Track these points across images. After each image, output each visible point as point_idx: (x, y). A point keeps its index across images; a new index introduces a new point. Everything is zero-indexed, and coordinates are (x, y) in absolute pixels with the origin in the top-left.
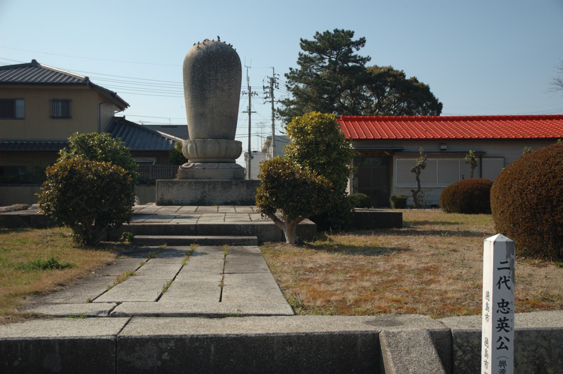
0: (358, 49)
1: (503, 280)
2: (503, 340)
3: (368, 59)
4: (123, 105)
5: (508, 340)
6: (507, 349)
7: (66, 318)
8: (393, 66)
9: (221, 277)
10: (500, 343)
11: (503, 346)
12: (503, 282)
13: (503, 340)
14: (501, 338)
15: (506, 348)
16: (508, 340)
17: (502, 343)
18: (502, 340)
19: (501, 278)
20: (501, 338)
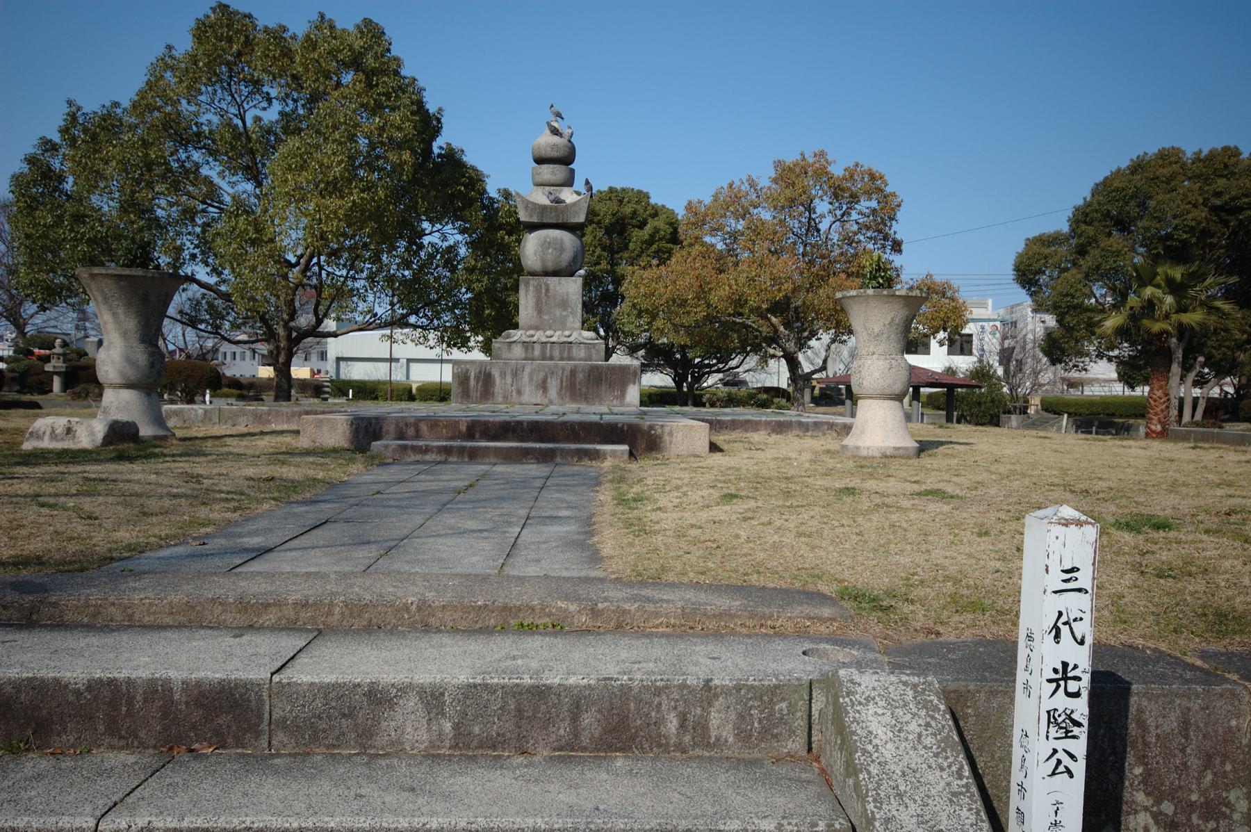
0: (941, 344)
1: (1064, 619)
2: (1061, 755)
3: (1201, 151)
4: (897, 247)
5: (1072, 756)
6: (1071, 776)
7: (169, 634)
8: (614, 185)
9: (508, 570)
10: (1053, 761)
11: (1061, 769)
12: (1064, 624)
13: (1061, 755)
14: (1055, 751)
15: (1069, 772)
16: (1072, 756)
17: (1059, 762)
18: (1057, 756)
19: (1060, 614)
20: (1055, 751)
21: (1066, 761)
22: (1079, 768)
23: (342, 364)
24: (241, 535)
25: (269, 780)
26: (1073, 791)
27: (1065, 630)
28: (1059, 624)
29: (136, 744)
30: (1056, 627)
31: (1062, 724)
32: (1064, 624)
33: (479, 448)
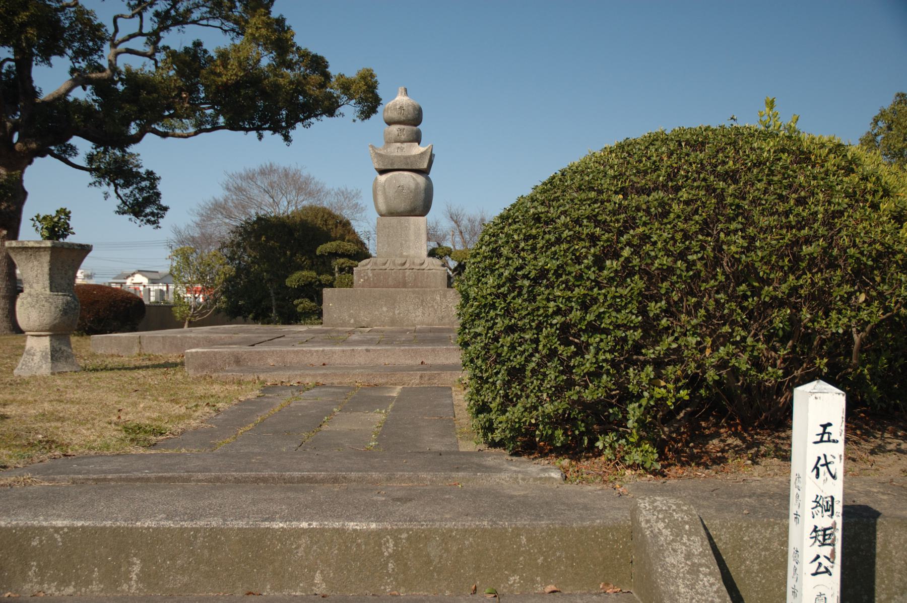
1: (822, 461)
10: (816, 564)
11: (822, 569)
12: (822, 465)
14: (818, 557)
15: (827, 571)
17: (820, 564)
18: (819, 560)
19: (819, 458)
20: (818, 557)
21: (826, 563)
22: (837, 570)
23: (119, 20)
24: (306, 332)
25: (281, 212)
26: (832, 585)
27: (823, 470)
28: (818, 466)
29: (53, 446)
30: (816, 467)
31: (823, 536)
32: (822, 465)
33: (204, 346)
